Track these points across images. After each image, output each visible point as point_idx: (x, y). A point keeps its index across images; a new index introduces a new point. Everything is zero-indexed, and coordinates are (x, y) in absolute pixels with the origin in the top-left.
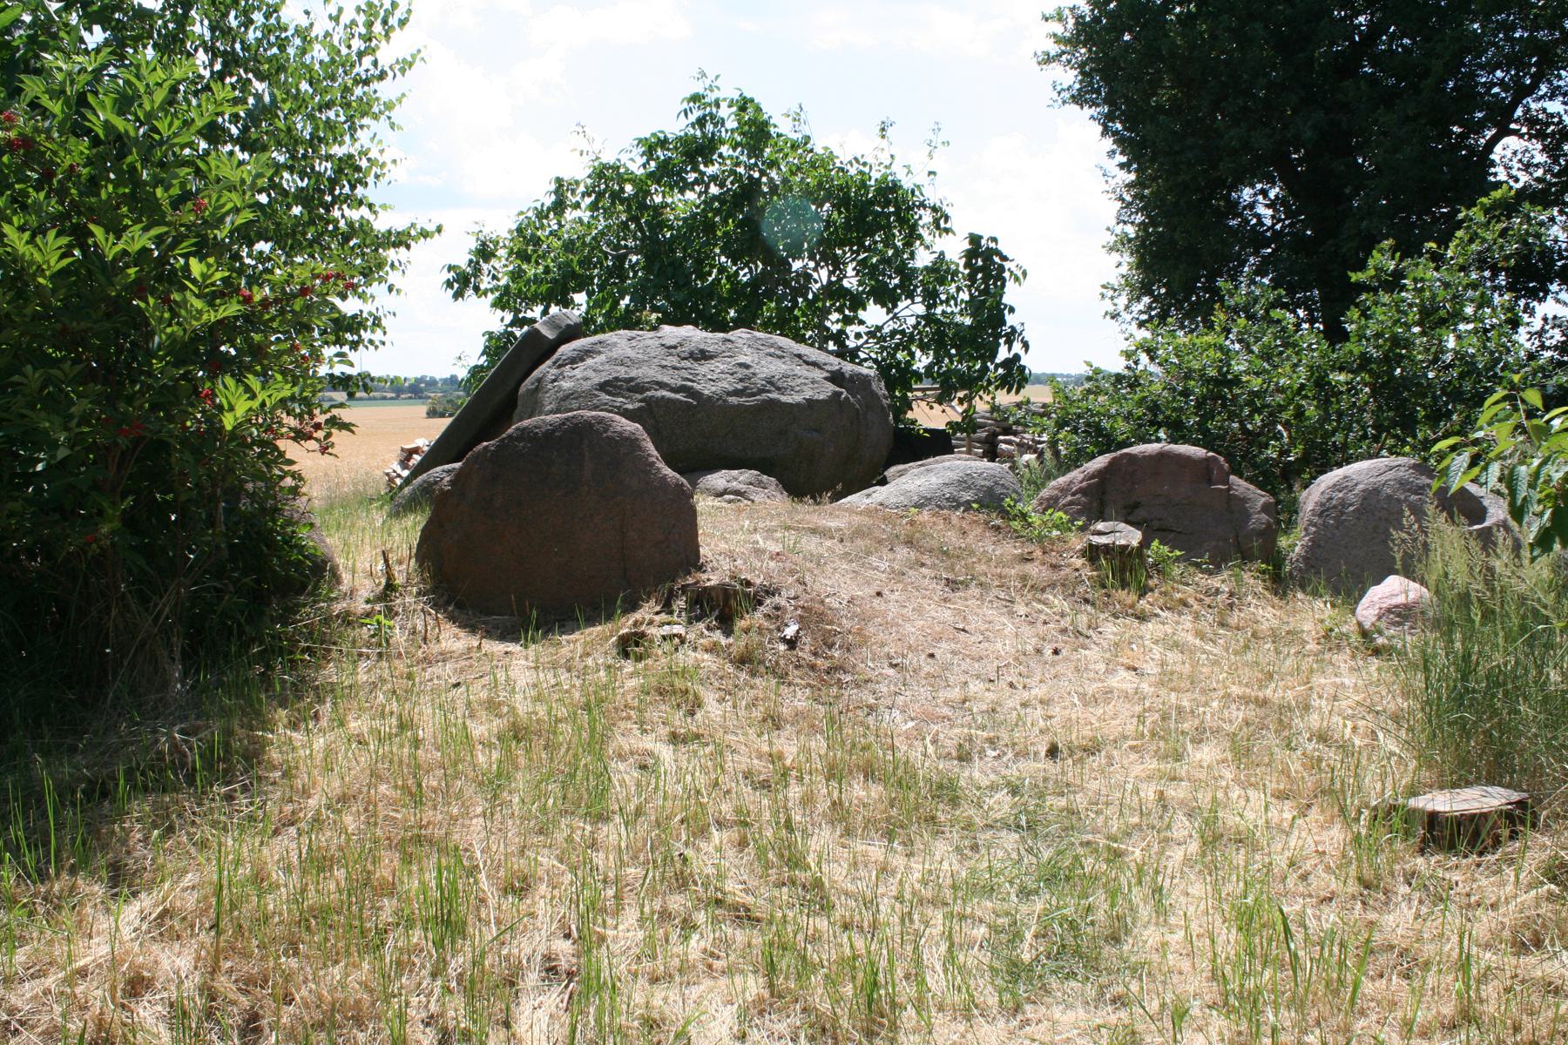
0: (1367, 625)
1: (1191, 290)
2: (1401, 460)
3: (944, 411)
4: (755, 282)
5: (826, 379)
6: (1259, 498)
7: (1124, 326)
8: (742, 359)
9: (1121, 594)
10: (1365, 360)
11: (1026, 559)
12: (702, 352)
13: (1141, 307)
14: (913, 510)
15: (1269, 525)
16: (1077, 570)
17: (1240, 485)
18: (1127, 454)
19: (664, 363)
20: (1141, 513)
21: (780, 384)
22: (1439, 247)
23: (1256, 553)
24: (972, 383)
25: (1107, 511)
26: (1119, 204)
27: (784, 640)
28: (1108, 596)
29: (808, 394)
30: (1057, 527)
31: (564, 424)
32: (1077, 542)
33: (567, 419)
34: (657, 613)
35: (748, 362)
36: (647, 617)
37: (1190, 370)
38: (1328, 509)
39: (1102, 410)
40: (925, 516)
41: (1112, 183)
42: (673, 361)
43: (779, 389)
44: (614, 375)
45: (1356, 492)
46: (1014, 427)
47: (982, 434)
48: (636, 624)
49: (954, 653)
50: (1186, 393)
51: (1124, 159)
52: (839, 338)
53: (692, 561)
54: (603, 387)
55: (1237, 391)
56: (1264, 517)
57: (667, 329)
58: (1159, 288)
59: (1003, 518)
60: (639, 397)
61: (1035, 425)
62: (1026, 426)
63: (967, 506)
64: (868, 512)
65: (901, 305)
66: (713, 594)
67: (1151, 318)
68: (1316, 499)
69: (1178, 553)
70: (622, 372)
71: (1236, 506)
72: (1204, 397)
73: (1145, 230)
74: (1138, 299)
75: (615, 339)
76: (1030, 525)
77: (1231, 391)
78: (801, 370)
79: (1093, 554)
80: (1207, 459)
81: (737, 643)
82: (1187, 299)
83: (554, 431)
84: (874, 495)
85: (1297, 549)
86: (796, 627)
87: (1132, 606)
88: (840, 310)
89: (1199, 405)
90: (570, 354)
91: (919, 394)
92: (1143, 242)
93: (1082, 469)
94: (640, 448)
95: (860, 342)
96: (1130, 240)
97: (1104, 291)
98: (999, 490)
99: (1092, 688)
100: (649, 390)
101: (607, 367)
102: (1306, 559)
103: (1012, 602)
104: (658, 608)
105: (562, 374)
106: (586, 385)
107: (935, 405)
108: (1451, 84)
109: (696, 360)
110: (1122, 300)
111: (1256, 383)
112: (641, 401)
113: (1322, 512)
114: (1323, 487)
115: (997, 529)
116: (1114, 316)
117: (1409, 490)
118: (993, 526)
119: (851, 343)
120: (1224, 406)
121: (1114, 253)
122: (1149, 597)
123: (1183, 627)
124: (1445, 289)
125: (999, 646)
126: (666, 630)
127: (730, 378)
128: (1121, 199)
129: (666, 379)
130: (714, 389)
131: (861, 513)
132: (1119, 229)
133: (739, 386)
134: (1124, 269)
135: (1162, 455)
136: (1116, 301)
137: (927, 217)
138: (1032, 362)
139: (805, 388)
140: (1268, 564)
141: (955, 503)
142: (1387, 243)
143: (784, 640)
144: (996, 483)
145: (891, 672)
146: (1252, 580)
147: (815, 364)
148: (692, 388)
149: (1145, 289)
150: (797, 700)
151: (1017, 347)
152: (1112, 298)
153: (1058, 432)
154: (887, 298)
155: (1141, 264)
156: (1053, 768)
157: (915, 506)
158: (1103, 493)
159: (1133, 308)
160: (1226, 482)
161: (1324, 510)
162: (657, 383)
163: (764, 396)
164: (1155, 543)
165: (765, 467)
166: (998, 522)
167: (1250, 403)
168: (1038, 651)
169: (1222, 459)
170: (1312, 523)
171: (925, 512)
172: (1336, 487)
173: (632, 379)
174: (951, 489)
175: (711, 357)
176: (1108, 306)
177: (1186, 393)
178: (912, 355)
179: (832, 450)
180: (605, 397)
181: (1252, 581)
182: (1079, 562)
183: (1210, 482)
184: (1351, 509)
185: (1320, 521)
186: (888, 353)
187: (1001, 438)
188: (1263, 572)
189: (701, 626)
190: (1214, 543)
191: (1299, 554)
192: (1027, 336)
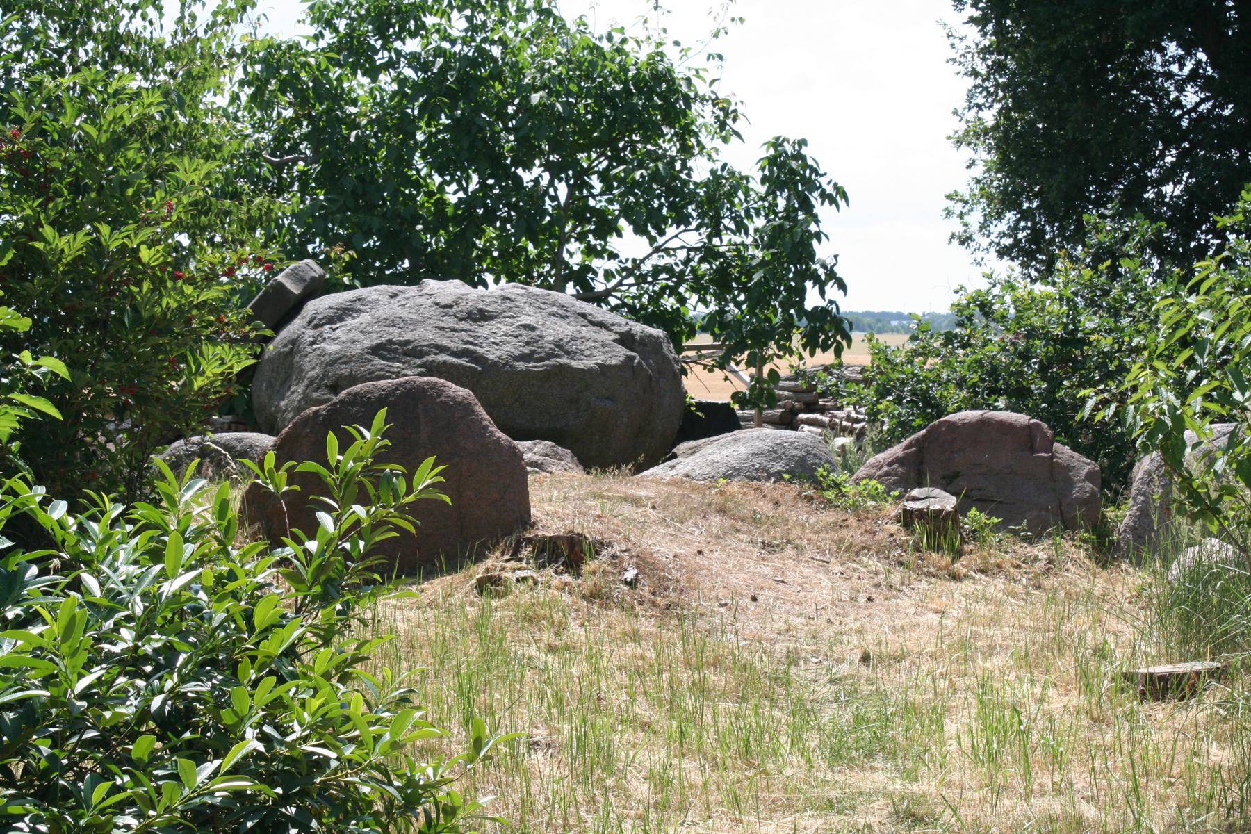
3: (726, 379)
4: (469, 203)
5: (615, 341)
6: (1084, 465)
7: (979, 255)
8: (526, 320)
9: (935, 556)
11: (843, 525)
12: (481, 311)
13: (1003, 226)
15: (1093, 493)
17: (1064, 452)
18: (945, 422)
19: (441, 324)
21: (568, 348)
26: (971, 82)
27: (626, 583)
29: (600, 359)
30: (873, 498)
31: (397, 389)
32: (892, 510)
33: (400, 384)
34: (507, 561)
35: (533, 323)
36: (499, 564)
37: (1033, 328)
39: (930, 375)
40: (735, 486)
41: (961, 46)
42: (449, 322)
43: (568, 353)
44: (386, 337)
46: (821, 402)
48: (487, 570)
49: (776, 599)
50: (1025, 356)
51: (976, 14)
52: (582, 276)
53: (525, 520)
54: (376, 350)
56: (1088, 486)
57: (431, 285)
60: (419, 362)
61: (850, 394)
62: (837, 395)
63: (778, 476)
64: (673, 483)
65: (671, 231)
66: (560, 543)
67: (1017, 242)
69: (996, 521)
70: (394, 334)
71: (1059, 475)
73: (1008, 118)
74: (1000, 216)
75: (374, 296)
76: (844, 495)
78: (587, 331)
79: (907, 519)
80: (1030, 426)
81: (587, 583)
83: (387, 396)
84: (679, 467)
86: (635, 572)
87: (947, 568)
88: (581, 238)
90: (326, 313)
91: (692, 353)
92: (1006, 132)
94: (473, 412)
95: (614, 282)
96: (986, 132)
97: (950, 204)
98: (811, 460)
99: (898, 623)
100: (428, 354)
101: (376, 328)
104: (507, 557)
105: (321, 335)
106: (356, 349)
108: (249, 824)
109: (475, 320)
110: (975, 218)
111: (1106, 343)
112: (420, 366)
115: (810, 499)
116: (965, 240)
118: (806, 497)
119: (599, 285)
121: (964, 148)
122: (964, 560)
123: (996, 587)
125: (816, 593)
126: (520, 574)
127: (515, 341)
128: (975, 73)
129: (445, 342)
130: (498, 353)
131: (668, 484)
133: (526, 350)
134: (978, 171)
136: (966, 219)
137: (703, 115)
138: (847, 305)
139: (595, 352)
143: (626, 583)
144: (808, 453)
145: (722, 609)
146: (1074, 550)
147: (601, 325)
148: (474, 352)
149: (1008, 200)
150: (647, 625)
151: (832, 291)
152: (961, 216)
153: (878, 402)
154: (648, 221)
155: (1004, 164)
156: (864, 670)
157: (724, 477)
158: (921, 463)
159: (992, 228)
160: (1049, 449)
162: (438, 347)
163: (553, 361)
164: (973, 511)
165: (559, 437)
166: (811, 492)
167: (1101, 367)
168: (853, 599)
169: (1045, 426)
171: (734, 484)
173: (408, 342)
175: (491, 318)
176: (956, 226)
178: (682, 301)
179: (625, 420)
180: (380, 363)
181: (1073, 549)
182: (893, 528)
183: (1032, 449)
186: (650, 297)
187: (802, 416)
188: (1085, 541)
189: (550, 571)
190: (1035, 513)
191: (1127, 525)
192: (840, 271)
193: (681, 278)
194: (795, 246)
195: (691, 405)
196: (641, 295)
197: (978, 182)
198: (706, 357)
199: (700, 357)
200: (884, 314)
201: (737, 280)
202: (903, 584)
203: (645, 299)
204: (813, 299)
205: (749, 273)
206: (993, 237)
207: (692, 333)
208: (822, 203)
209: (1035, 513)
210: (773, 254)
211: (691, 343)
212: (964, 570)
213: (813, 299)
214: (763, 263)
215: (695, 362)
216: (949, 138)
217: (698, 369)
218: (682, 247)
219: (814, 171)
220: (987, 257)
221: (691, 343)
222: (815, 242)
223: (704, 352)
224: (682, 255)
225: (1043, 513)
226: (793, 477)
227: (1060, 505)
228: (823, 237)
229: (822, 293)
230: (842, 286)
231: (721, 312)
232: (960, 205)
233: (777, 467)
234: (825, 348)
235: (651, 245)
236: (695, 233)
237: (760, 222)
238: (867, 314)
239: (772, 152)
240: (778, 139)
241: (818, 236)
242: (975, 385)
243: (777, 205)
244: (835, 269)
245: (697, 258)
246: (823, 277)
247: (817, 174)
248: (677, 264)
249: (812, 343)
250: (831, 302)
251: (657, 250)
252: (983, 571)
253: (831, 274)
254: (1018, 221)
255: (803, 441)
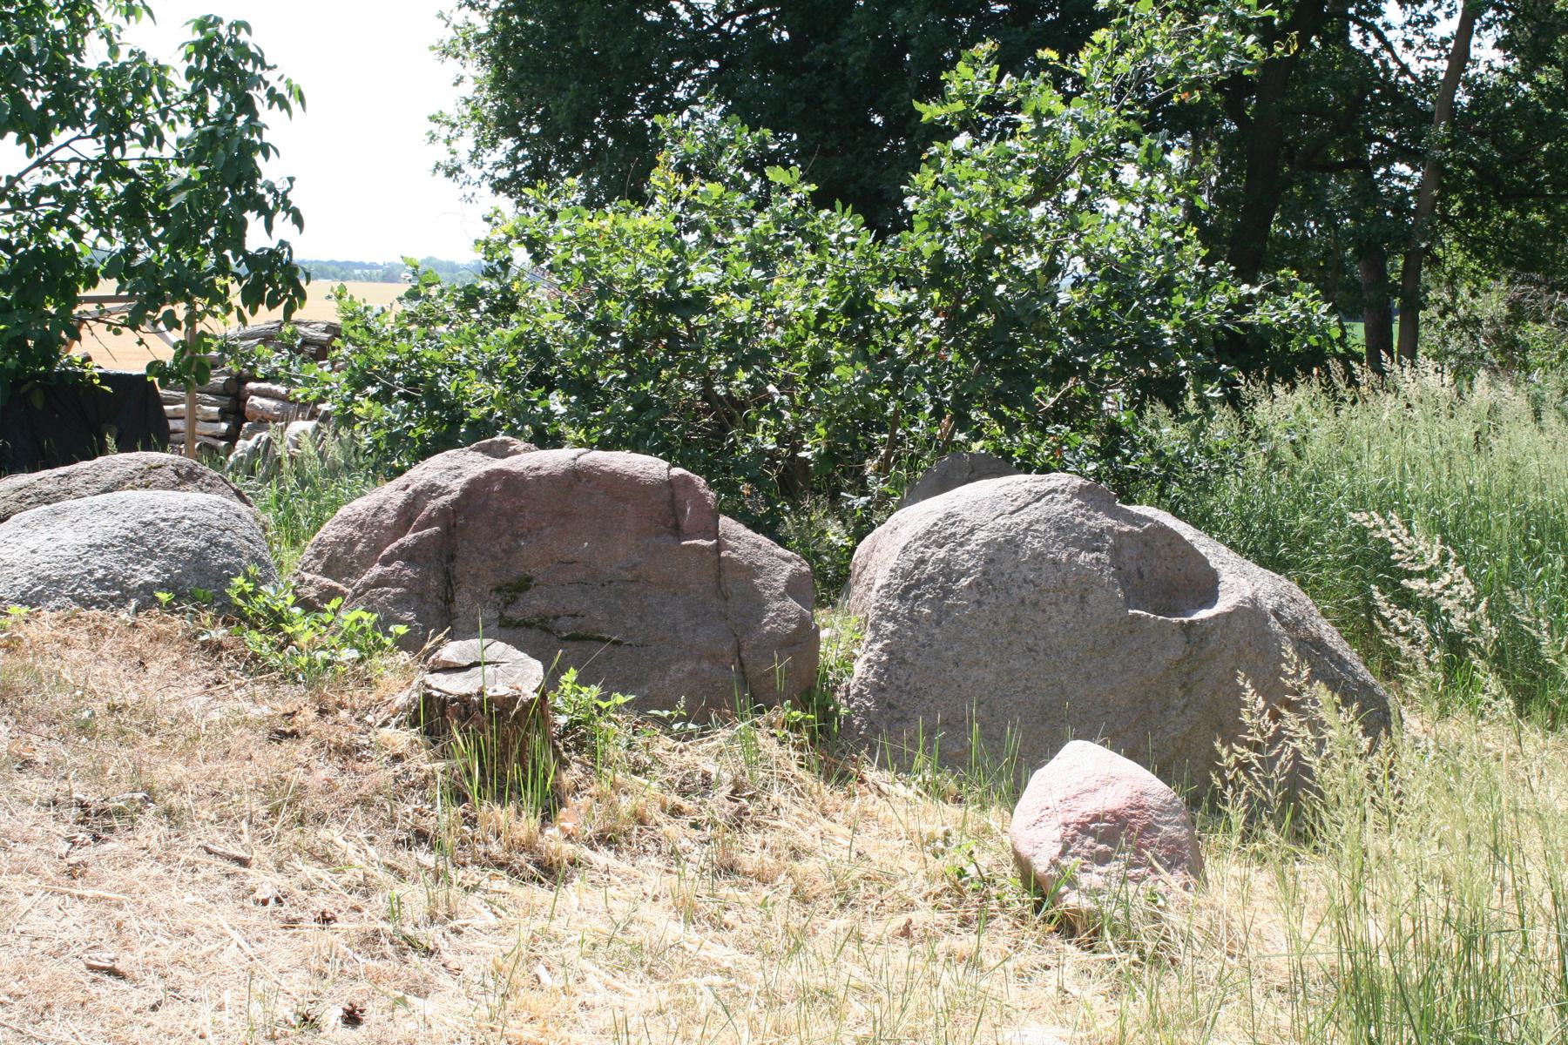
0: (1041, 865)
1: (582, 127)
2: (1056, 479)
3: (141, 342)
7: (469, 190)
9: (502, 815)
10: (942, 269)
13: (499, 155)
14: (17, 610)
16: (398, 758)
20: (533, 603)
22: (1062, 59)
23: (780, 684)
24: (190, 285)
25: (463, 598)
28: (473, 822)
30: (348, 639)
38: (918, 584)
40: (44, 626)
45: (972, 546)
47: (218, 380)
55: (699, 320)
58: (529, 123)
59: (227, 623)
65: (59, 138)
68: (892, 563)
72: (639, 336)
73: (505, 21)
74: (494, 144)
77: (686, 321)
80: (671, 483)
82: (577, 146)
85: (859, 668)
89: (629, 348)
91: (91, 307)
92: (503, 42)
93: (401, 481)
96: (479, 39)
97: (435, 127)
102: (878, 690)
103: (243, 862)
107: (126, 330)
110: (466, 144)
113: (907, 589)
114: (904, 537)
115: (216, 649)
117: (1075, 542)
118: (204, 645)
120: (672, 349)
121: (450, 59)
124: (1084, 136)
132: (459, 17)
134: (468, 89)
135: (577, 476)
136: (454, 145)
138: (304, 250)
140: (805, 710)
141: (113, 592)
142: (984, 48)
149: (507, 124)
151: (283, 226)
158: (451, 558)
159: (485, 158)
161: (909, 585)
166: (219, 634)
167: (726, 347)
169: (700, 481)
170: (886, 614)
172: (933, 537)
174: (109, 558)
176: (441, 154)
177: (603, 327)
178: (77, 235)
182: (401, 738)
183: (678, 532)
184: (964, 582)
185: (904, 610)
186: (32, 229)
187: (252, 385)
188: (796, 728)
190: (689, 666)
193: (70, 202)
194: (230, 162)
195: (93, 377)
196: (20, 226)
197: (467, 102)
198: (110, 313)
199: (102, 312)
200: (347, 263)
201: (153, 208)
202: (432, 918)
203: (25, 232)
204: (256, 238)
205: (165, 196)
206: (486, 168)
207: (92, 281)
208: (270, 107)
209: (689, 666)
210: (202, 172)
211: (91, 293)
212: (568, 849)
213: (256, 238)
214: (187, 184)
215: (97, 320)
216: (432, 48)
217: (100, 328)
218: (74, 160)
219: (259, 61)
220: (478, 192)
221: (91, 293)
222: (259, 158)
223: (107, 306)
224: (74, 169)
225: (705, 665)
226: (179, 596)
227: (739, 650)
228: (272, 152)
229: (269, 227)
230: (298, 220)
231: (130, 252)
232: (447, 129)
233: (145, 574)
234: (272, 305)
235: (29, 154)
236: (93, 142)
237: (185, 130)
238: (332, 263)
239: (198, 36)
240: (208, 17)
241: (265, 149)
242: (511, 371)
243: (206, 109)
244: (290, 196)
245: (94, 175)
246: (271, 205)
247: (264, 66)
248: (66, 184)
249: (253, 297)
250: (283, 244)
251: (41, 163)
252: (606, 839)
253: (284, 203)
254: (519, 148)
255: (200, 516)
